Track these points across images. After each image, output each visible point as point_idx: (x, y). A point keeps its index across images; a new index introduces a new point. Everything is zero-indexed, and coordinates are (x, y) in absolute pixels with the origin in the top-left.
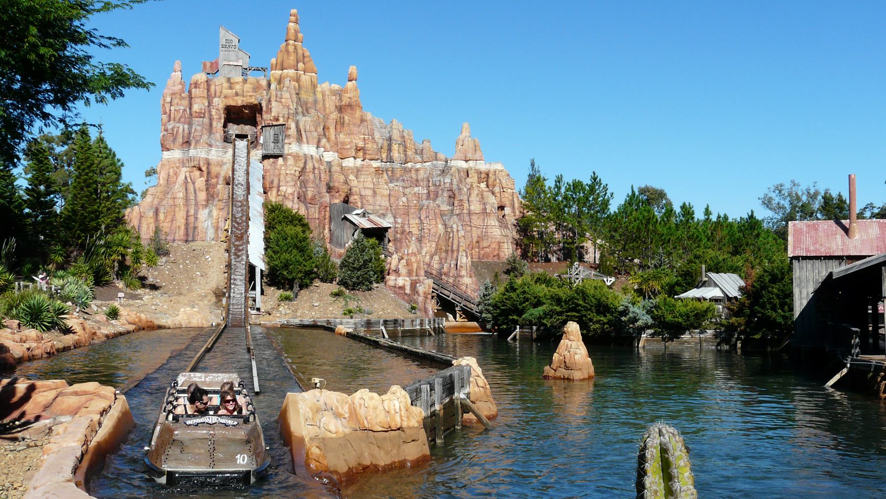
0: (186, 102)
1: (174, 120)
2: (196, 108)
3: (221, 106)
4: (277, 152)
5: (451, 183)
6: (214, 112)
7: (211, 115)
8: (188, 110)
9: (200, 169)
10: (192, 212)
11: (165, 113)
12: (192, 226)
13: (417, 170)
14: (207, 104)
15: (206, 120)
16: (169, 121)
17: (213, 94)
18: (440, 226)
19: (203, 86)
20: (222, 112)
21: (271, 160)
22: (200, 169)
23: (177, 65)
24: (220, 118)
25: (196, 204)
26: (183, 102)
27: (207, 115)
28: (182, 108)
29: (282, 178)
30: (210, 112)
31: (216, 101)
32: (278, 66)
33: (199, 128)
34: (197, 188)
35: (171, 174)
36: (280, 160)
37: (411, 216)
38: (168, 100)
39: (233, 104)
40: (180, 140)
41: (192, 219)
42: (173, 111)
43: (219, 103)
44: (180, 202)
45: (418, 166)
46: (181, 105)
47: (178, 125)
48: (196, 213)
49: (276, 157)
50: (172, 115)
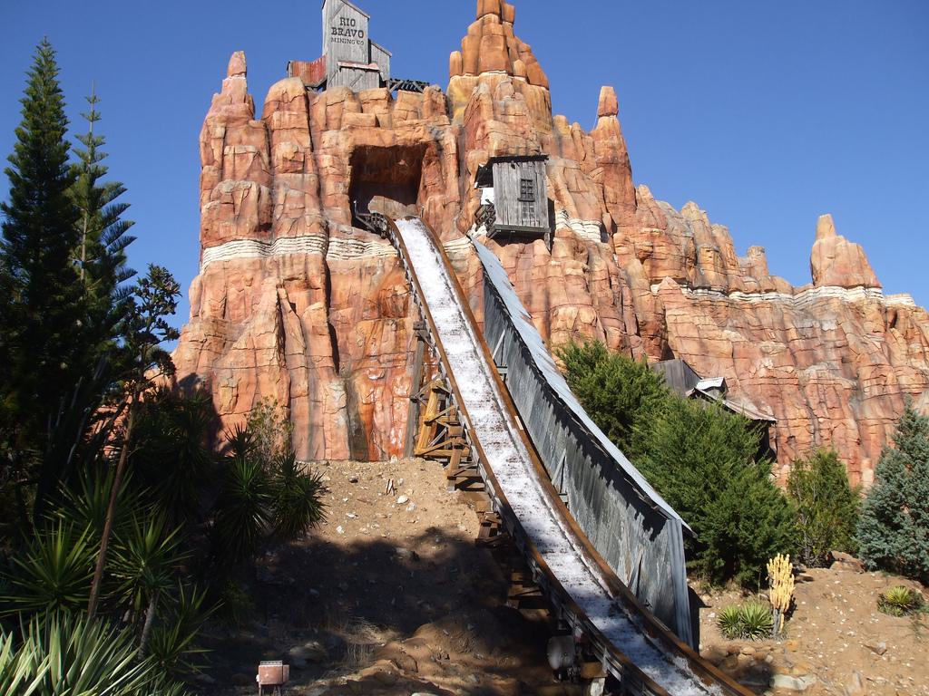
0: (259, 139)
1: (234, 177)
2: (283, 149)
3: (345, 146)
4: (530, 223)
5: (840, 331)
6: (326, 161)
7: (318, 169)
8: (265, 154)
9: (308, 285)
10: (302, 385)
11: (211, 162)
12: (302, 422)
13: (754, 307)
14: (307, 144)
15: (310, 177)
16: (221, 178)
17: (321, 123)
18: (851, 423)
19: (299, 104)
20: (346, 160)
21: (517, 247)
22: (308, 285)
23: (237, 61)
24: (342, 175)
25: (309, 367)
26: (253, 138)
27: (310, 166)
28: (251, 148)
29: (555, 287)
30: (316, 161)
31: (328, 137)
32: (469, 66)
33: (294, 193)
34: (309, 326)
35: (231, 298)
36: (540, 246)
37: (787, 401)
38: (219, 131)
39: (375, 142)
40: (251, 218)
41: (301, 406)
42: (229, 158)
43: (337, 143)
44: (269, 357)
45: (755, 299)
46: (249, 143)
47: (244, 184)
48: (312, 389)
49: (527, 237)
50: (228, 167)
